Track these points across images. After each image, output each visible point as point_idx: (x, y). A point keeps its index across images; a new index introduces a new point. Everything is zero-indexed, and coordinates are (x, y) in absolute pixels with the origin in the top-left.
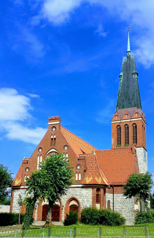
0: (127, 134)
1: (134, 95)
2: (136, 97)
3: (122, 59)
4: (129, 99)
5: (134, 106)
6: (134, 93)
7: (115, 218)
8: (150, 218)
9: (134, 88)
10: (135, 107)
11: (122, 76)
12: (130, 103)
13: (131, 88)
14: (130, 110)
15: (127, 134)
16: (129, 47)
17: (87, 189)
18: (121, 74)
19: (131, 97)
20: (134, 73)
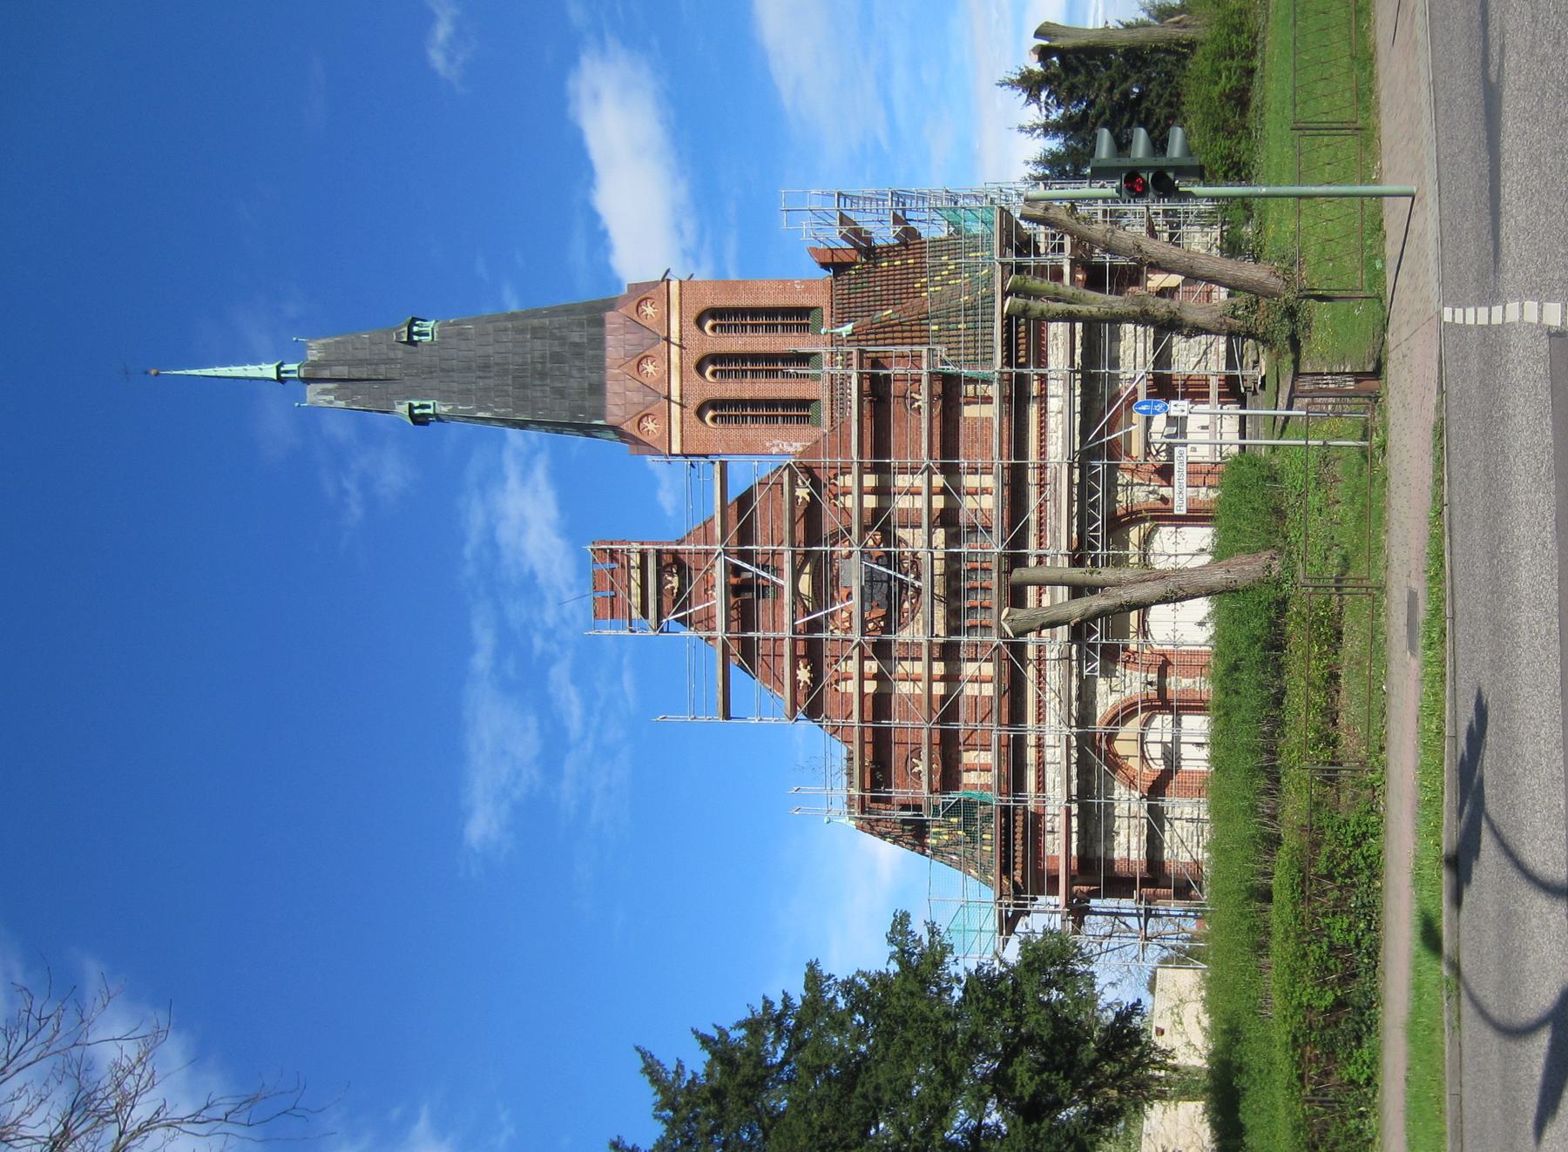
0: (770, 363)
1: (534, 330)
2: (547, 321)
3: (316, 410)
4: (557, 358)
5: (593, 330)
6: (522, 331)
7: (887, 536)
8: (856, 263)
9: (497, 330)
10: (601, 323)
11: (416, 403)
12: (578, 350)
13: (490, 350)
14: (615, 347)
15: (770, 363)
16: (252, 371)
17: (1479, 1018)
18: (402, 409)
19: (540, 347)
20: (410, 334)
